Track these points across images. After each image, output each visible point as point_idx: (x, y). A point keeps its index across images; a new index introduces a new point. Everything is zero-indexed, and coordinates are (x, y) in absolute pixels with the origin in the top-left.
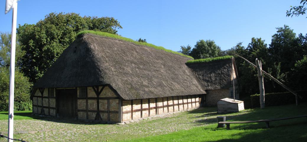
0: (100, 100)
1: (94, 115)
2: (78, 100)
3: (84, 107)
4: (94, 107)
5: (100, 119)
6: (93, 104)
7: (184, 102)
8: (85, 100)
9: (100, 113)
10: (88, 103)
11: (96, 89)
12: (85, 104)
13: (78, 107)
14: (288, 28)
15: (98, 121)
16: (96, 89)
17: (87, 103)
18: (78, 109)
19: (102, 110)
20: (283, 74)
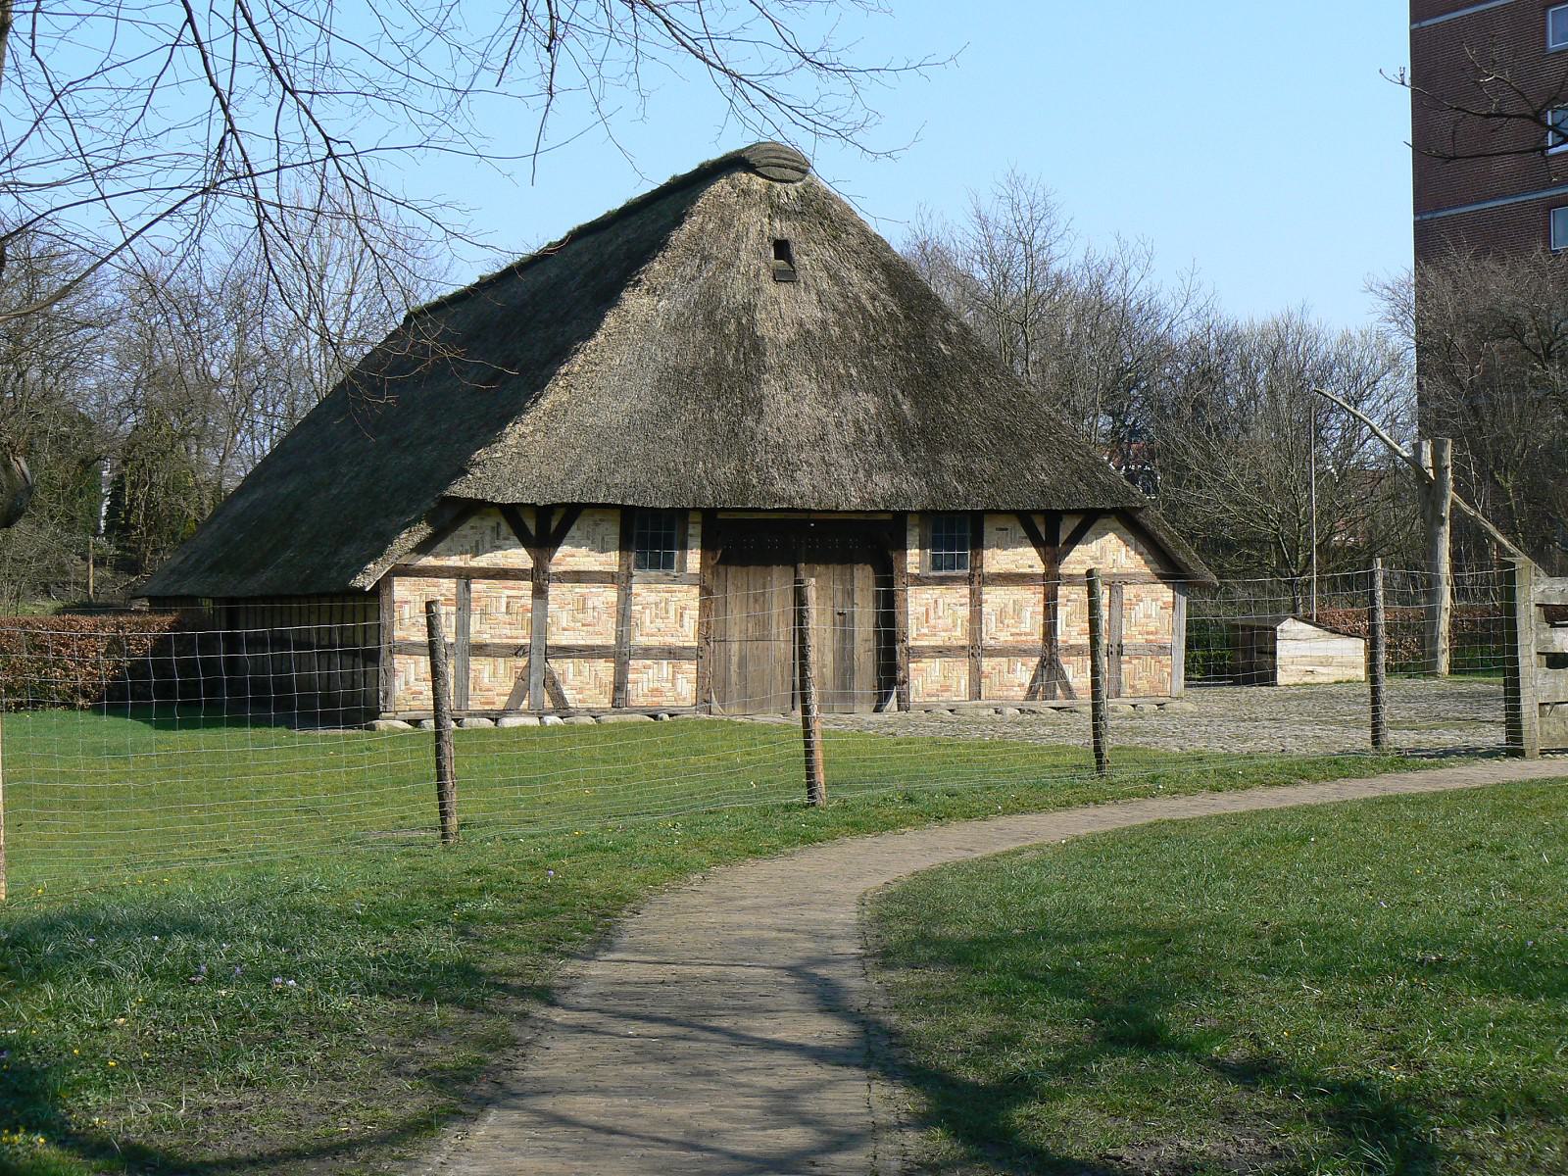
0: (1062, 591)
1: (1410, 640)
2: (911, 590)
3: (958, 633)
4: (1026, 627)
5: (1059, 691)
6: (1018, 611)
7: (994, 633)
8: (965, 590)
9: (1062, 660)
10: (986, 609)
11: (1042, 529)
12: (965, 612)
13: (912, 632)
14: (1332, 356)
15: (1248, 681)
16: (1042, 529)
17: (976, 602)
18: (911, 643)
19: (1071, 642)
20: (367, 589)
